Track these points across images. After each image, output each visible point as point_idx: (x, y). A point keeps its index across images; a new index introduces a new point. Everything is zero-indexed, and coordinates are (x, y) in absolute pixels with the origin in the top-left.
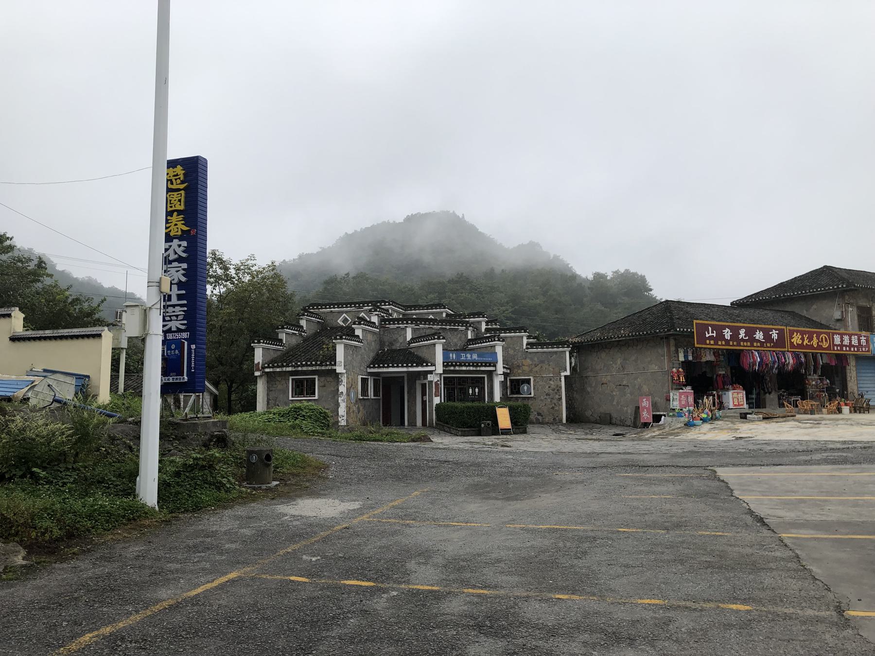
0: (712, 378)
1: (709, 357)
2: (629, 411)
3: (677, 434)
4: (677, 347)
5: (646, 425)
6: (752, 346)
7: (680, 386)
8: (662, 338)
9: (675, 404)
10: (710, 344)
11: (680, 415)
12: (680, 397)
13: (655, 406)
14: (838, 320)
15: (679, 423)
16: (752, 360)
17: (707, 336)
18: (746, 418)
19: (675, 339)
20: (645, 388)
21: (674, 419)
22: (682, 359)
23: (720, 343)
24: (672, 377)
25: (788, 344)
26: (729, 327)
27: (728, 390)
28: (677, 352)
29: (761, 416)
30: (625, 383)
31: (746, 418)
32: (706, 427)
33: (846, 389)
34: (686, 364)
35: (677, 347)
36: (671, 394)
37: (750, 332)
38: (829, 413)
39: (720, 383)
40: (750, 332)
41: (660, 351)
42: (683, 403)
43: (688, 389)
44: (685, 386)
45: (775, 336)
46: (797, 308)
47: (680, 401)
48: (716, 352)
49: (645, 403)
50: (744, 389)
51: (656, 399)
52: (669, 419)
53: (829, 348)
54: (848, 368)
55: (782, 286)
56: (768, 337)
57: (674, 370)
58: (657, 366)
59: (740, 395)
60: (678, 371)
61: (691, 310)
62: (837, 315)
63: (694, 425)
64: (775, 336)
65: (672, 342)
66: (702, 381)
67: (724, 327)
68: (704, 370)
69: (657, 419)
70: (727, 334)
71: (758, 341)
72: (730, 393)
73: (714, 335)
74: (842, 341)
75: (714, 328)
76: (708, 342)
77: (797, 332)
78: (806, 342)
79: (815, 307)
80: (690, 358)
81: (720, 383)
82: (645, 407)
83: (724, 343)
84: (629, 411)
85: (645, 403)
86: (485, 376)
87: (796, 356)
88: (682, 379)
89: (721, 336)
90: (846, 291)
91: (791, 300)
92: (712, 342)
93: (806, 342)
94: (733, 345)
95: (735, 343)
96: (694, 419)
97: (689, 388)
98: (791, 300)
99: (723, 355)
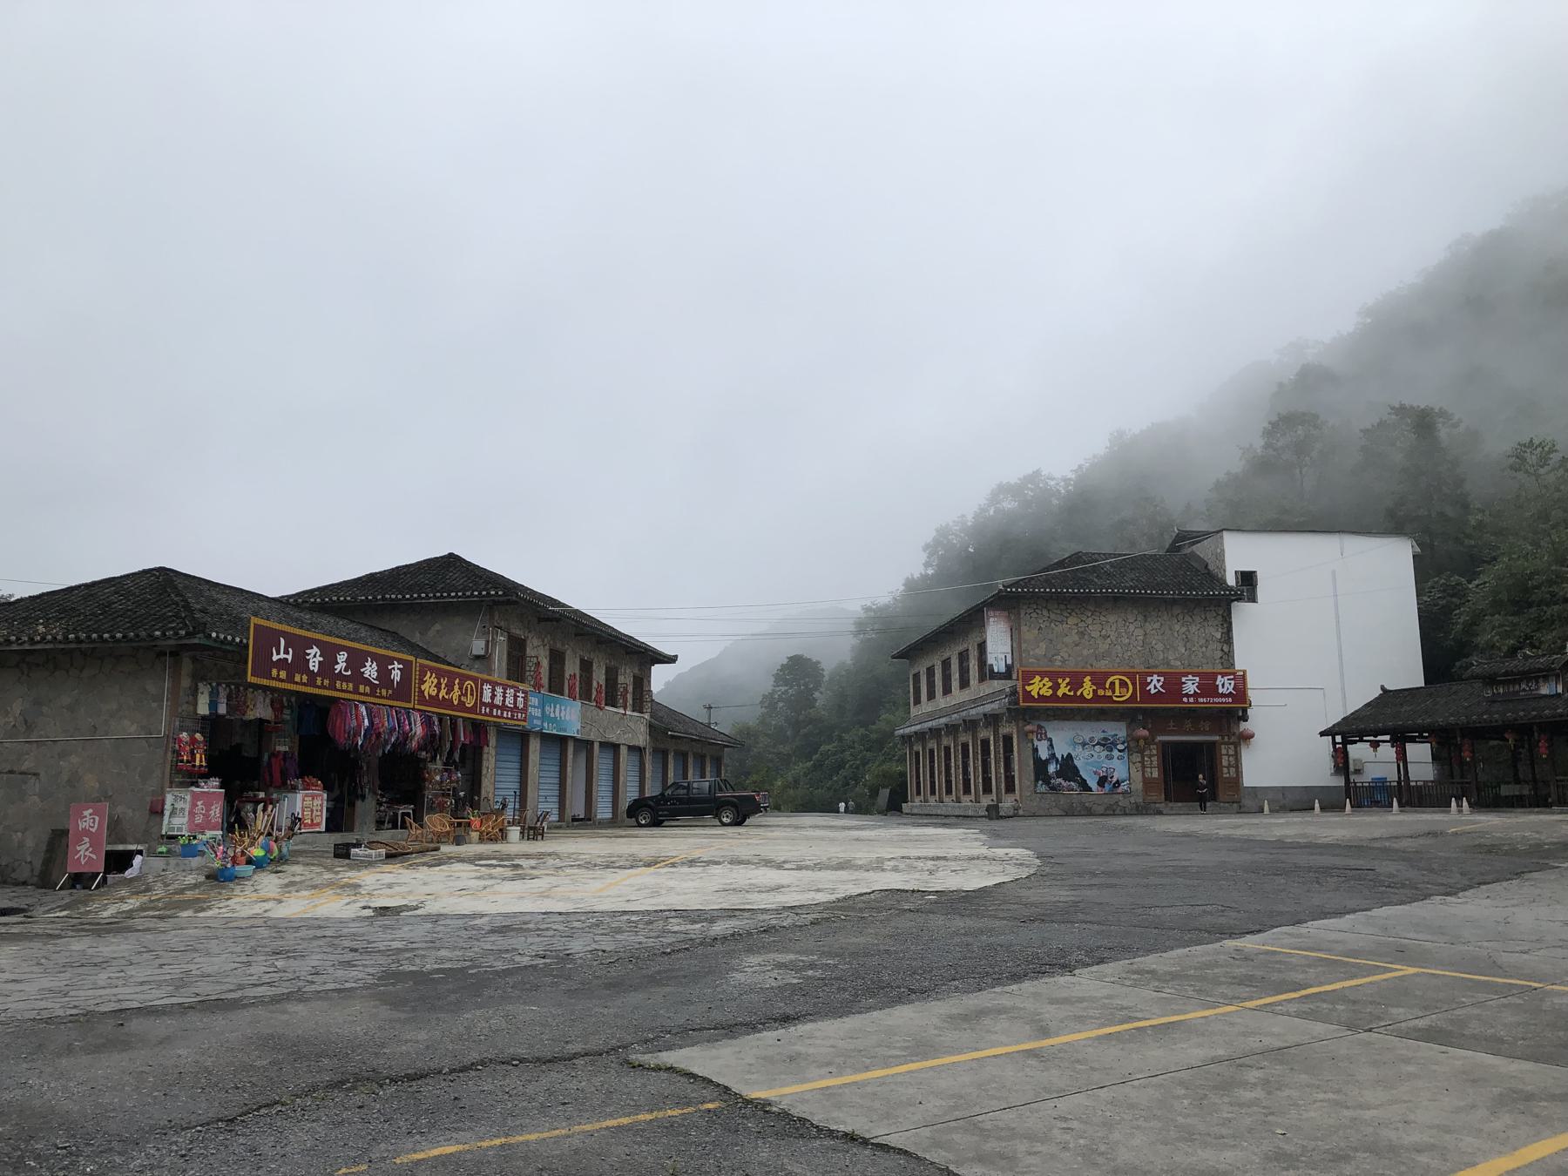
0: (258, 759)
1: (260, 710)
2: (30, 843)
3: (198, 905)
4: (198, 677)
5: (80, 880)
6: (356, 691)
7: (191, 778)
8: (162, 654)
9: (176, 822)
10: (278, 679)
11: (190, 851)
12: (194, 805)
13: (115, 829)
14: (478, 657)
15: (189, 875)
16: (354, 723)
17: (275, 658)
18: (347, 856)
19: (194, 660)
20: (90, 782)
21: (173, 861)
22: (203, 709)
23: (297, 678)
24: (177, 753)
25: (414, 695)
26: (318, 643)
27: (294, 789)
28: (195, 692)
29: (383, 851)
30: (26, 765)
31: (347, 856)
32: (269, 883)
33: (479, 794)
34: (213, 726)
35: (198, 677)
36: (169, 799)
37: (356, 660)
38: (481, 840)
39: (277, 775)
40: (356, 660)
41: (151, 688)
42: (199, 820)
43: (212, 786)
44: (206, 776)
45: (396, 675)
46: (403, 626)
47: (192, 814)
48: (278, 699)
49: (89, 820)
50: (326, 788)
51: (119, 809)
52: (158, 863)
53: (473, 710)
54: (486, 749)
55: (372, 580)
56: (384, 673)
57: (184, 735)
58: (148, 717)
59: (317, 802)
60: (193, 741)
61: (223, 599)
62: (478, 647)
63: (234, 878)
64: (396, 675)
65: (187, 666)
66: (240, 768)
67: (310, 643)
68: (237, 740)
69: (118, 862)
70: (314, 658)
71: (367, 682)
72: (299, 796)
73: (290, 657)
74: (493, 696)
75: (292, 641)
76: (274, 672)
77: (432, 670)
78: (443, 693)
79: (437, 627)
80: (222, 710)
81: (277, 775)
82: (86, 832)
83: (305, 678)
84: (30, 843)
85: (89, 820)
86: (250, 679)
87: (427, 722)
88: (200, 760)
89: (301, 663)
90: (496, 603)
91: (394, 608)
92: (283, 674)
93: (443, 693)
94: (322, 687)
95: (326, 682)
96: (234, 861)
97: (215, 782)
98: (394, 608)
99: (290, 707)
